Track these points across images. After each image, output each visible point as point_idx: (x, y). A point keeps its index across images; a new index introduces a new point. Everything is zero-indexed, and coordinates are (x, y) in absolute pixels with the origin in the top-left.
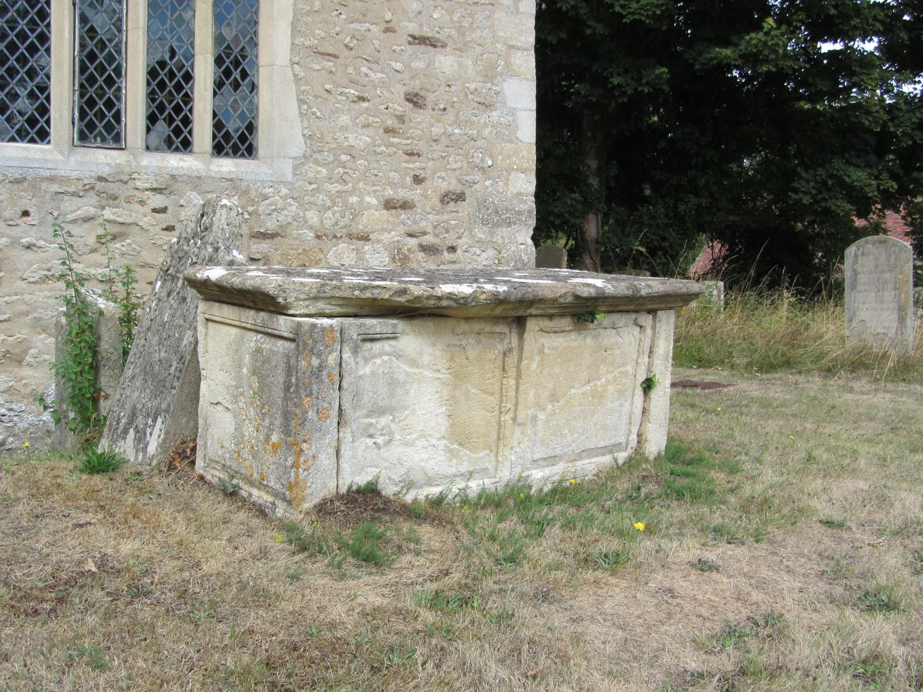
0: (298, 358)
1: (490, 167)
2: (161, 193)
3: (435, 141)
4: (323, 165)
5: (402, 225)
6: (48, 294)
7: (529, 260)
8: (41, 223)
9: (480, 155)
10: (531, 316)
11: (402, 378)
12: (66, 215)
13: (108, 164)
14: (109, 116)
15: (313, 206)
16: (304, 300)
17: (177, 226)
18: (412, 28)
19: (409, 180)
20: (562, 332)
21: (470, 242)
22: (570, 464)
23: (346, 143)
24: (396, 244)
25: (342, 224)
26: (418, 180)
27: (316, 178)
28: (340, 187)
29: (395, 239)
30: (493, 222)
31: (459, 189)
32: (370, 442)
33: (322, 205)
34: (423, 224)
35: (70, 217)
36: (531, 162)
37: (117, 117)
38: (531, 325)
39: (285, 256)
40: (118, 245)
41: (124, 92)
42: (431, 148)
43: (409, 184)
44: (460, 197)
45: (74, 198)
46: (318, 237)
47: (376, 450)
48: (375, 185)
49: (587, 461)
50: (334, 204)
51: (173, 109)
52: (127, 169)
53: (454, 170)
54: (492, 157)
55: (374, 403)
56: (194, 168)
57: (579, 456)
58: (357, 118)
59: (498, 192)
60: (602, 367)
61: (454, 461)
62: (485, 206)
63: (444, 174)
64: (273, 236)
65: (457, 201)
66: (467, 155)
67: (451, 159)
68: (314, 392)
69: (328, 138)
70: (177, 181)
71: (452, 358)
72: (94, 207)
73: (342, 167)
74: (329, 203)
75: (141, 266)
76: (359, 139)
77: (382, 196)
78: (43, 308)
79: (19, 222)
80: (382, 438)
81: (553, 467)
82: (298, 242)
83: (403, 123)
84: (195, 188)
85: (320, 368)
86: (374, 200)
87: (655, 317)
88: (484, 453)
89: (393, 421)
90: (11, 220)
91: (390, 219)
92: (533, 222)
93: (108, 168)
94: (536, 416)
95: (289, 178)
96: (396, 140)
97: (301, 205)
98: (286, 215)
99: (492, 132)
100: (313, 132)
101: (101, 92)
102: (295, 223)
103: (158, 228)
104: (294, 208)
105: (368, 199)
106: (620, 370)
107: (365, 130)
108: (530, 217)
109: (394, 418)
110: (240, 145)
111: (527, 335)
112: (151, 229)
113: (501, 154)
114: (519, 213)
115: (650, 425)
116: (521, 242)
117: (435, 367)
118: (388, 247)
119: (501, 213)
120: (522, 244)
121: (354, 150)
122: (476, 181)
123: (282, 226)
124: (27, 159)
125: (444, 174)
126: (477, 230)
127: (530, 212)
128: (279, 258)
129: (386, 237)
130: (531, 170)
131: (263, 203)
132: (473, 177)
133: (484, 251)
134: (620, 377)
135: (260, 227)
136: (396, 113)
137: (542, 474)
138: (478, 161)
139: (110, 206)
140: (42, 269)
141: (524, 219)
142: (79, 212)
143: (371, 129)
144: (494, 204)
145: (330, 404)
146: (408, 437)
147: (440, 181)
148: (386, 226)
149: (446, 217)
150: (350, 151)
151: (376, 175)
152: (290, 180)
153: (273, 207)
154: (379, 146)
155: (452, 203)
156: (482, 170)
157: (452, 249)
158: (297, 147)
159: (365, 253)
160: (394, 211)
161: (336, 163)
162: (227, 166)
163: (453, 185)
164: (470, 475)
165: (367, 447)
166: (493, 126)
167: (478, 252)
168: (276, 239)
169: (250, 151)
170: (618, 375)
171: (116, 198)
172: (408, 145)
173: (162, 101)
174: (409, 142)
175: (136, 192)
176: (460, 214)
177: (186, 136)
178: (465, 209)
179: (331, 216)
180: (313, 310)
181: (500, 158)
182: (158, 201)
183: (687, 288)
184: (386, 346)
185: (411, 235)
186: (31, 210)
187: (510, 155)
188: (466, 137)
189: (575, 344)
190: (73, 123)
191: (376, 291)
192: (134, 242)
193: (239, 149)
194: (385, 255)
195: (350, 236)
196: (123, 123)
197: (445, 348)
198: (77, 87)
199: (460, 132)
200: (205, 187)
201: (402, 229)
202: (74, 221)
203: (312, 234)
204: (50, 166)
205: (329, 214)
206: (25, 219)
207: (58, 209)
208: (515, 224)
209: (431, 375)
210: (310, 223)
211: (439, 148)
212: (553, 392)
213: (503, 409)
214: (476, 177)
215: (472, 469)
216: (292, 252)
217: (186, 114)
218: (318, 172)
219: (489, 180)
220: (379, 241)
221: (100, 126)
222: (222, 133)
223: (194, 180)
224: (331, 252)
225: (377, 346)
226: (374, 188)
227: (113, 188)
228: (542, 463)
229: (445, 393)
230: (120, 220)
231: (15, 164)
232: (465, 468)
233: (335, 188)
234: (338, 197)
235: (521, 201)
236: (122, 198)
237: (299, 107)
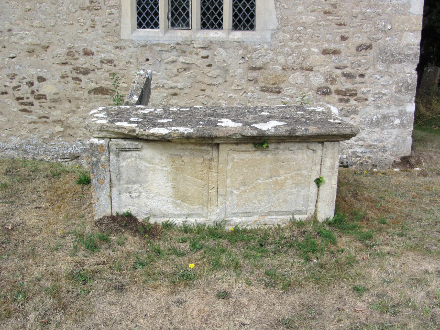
1: (389, 30)
2: (206, 49)
3: (355, 17)
4: (288, 33)
5: (333, 63)
6: (157, 94)
7: (413, 82)
8: (154, 64)
9: (383, 23)
10: (222, 143)
11: (143, 168)
12: (164, 60)
13: (182, 37)
14: (184, 14)
15: (282, 54)
16: (97, 131)
17: (213, 64)
19: (338, 38)
20: (249, 151)
21: (373, 72)
22: (260, 217)
23: (301, 21)
24: (328, 73)
25: (297, 62)
26: (343, 38)
27: (284, 40)
28: (297, 44)
29: (328, 70)
30: (389, 61)
31: (368, 43)
32: (128, 195)
33: (286, 53)
34: (345, 62)
35: (166, 61)
36: (418, 26)
37: (187, 15)
38: (221, 147)
39: (266, 78)
40: (187, 73)
41: (190, 3)
42: (353, 21)
43: (338, 41)
44: (369, 47)
45: (167, 53)
46: (284, 69)
47: (131, 199)
48: (318, 42)
49: (274, 217)
50: (293, 52)
51: (214, 9)
52: (190, 39)
53: (366, 32)
54: (391, 24)
55: (128, 179)
56: (221, 37)
57: (269, 214)
58: (308, 7)
59: (394, 44)
60: (281, 170)
61: (179, 208)
62: (385, 52)
63: (360, 35)
64: (259, 69)
65: (366, 49)
66: (375, 23)
67: (364, 26)
68: (95, 172)
69: (291, 18)
70: (213, 43)
71: (173, 161)
72: (176, 56)
73: (299, 33)
74: (290, 52)
75: (197, 82)
76: (310, 18)
77: (321, 48)
78: (155, 100)
79: (145, 63)
80: (135, 194)
81: (249, 218)
82: (273, 72)
83: (336, 8)
84: (221, 47)
85: (97, 162)
86: (317, 49)
87: (323, 145)
88: (198, 206)
89: (140, 187)
90: (142, 62)
91: (326, 59)
92: (417, 61)
93: (181, 39)
94: (232, 192)
95: (269, 40)
96: (331, 18)
97: (275, 53)
98: (267, 59)
99: (392, 10)
100: (282, 16)
101: (180, 4)
102: (271, 62)
103: (204, 65)
104: (271, 55)
105: (313, 49)
106: (296, 172)
107: (312, 13)
108: (415, 57)
109: (141, 186)
110: (246, 24)
111: (221, 152)
112: (201, 66)
113: (397, 22)
114: (407, 56)
115: (320, 203)
116: (407, 72)
117: (163, 165)
118: (324, 74)
119: (395, 55)
120: (409, 73)
121: (306, 24)
122: (380, 38)
123: (264, 64)
124: (147, 36)
125: (360, 35)
126: (378, 65)
127: (415, 55)
128: (262, 80)
129: (322, 69)
130: (418, 30)
131: (255, 53)
132: (377, 36)
133: (382, 77)
134: (296, 176)
135: (253, 64)
136: (331, 3)
137: (240, 220)
138: (381, 27)
139: (182, 56)
140: (155, 83)
141: (411, 59)
142: (169, 59)
143: (316, 13)
144: (391, 50)
145: (104, 177)
146: (150, 195)
147: (357, 38)
148: (323, 63)
149: (359, 58)
150: (303, 25)
151: (318, 37)
152: (269, 41)
153: (260, 55)
154: (320, 21)
155: (363, 51)
156: (384, 31)
157: (362, 76)
158: (274, 24)
159: (310, 77)
160: (328, 55)
161: (295, 31)
162: (238, 35)
163: (365, 41)
164: (189, 215)
165: (127, 197)
166: (393, 6)
167: (378, 77)
168: (261, 70)
169: (252, 27)
170: (294, 175)
171: (185, 52)
172: (338, 20)
173: (208, 6)
174: (339, 18)
175: (194, 49)
176: (368, 57)
177: (220, 22)
178: (371, 54)
179: (291, 58)
180: (101, 135)
181: (397, 24)
182: (204, 53)
183: (339, 131)
184: (134, 154)
185: (337, 68)
186: (149, 59)
187: (404, 23)
188: (375, 14)
189: (259, 158)
190: (168, 19)
191: (123, 130)
192: (194, 72)
193: (246, 26)
194: (322, 78)
195: (302, 69)
196: (190, 18)
197: (169, 156)
198: (170, 3)
199: (371, 11)
200: (226, 46)
201: (333, 65)
202: (167, 63)
203: (280, 68)
204: (157, 39)
205: (290, 57)
206: (147, 62)
207: (161, 57)
208: (404, 61)
209: (160, 168)
210: (279, 62)
211: (357, 20)
212: (243, 181)
213: (210, 187)
214: (380, 36)
215: (190, 213)
216: (269, 77)
217: (220, 11)
218: (285, 37)
219: (389, 37)
220: (318, 71)
221: (180, 19)
222: (237, 19)
223: (221, 43)
224: (291, 77)
225: (129, 154)
226: (317, 43)
227: (184, 48)
228: (241, 215)
229: (170, 177)
230: (187, 62)
231: (143, 39)
232: (185, 212)
233: (293, 44)
234: (296, 49)
235: (410, 49)
236: (188, 52)
237: (275, 4)
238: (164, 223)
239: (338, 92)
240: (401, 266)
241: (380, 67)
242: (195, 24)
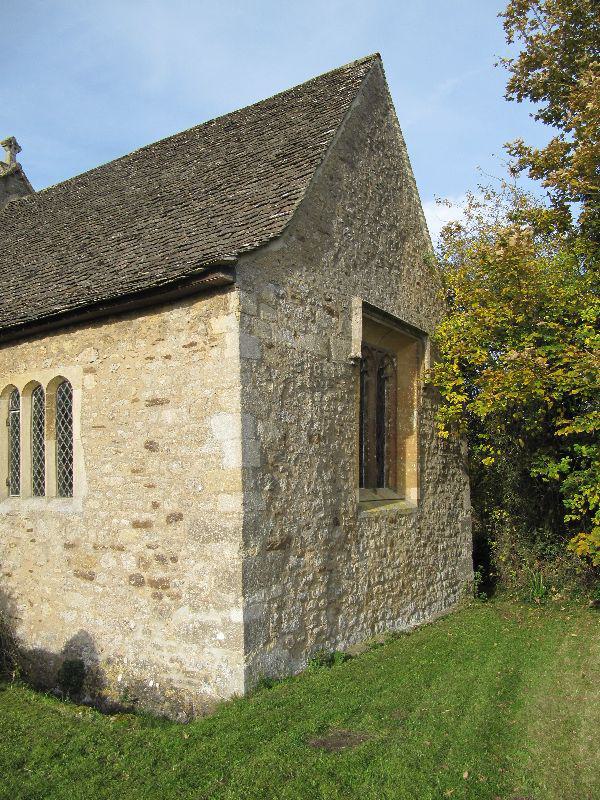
0: (255, 250)
18: (148, 395)
19: (150, 505)
76: (116, 481)
105: (123, 521)
178: (181, 528)
195: (112, 547)
239: (154, 584)
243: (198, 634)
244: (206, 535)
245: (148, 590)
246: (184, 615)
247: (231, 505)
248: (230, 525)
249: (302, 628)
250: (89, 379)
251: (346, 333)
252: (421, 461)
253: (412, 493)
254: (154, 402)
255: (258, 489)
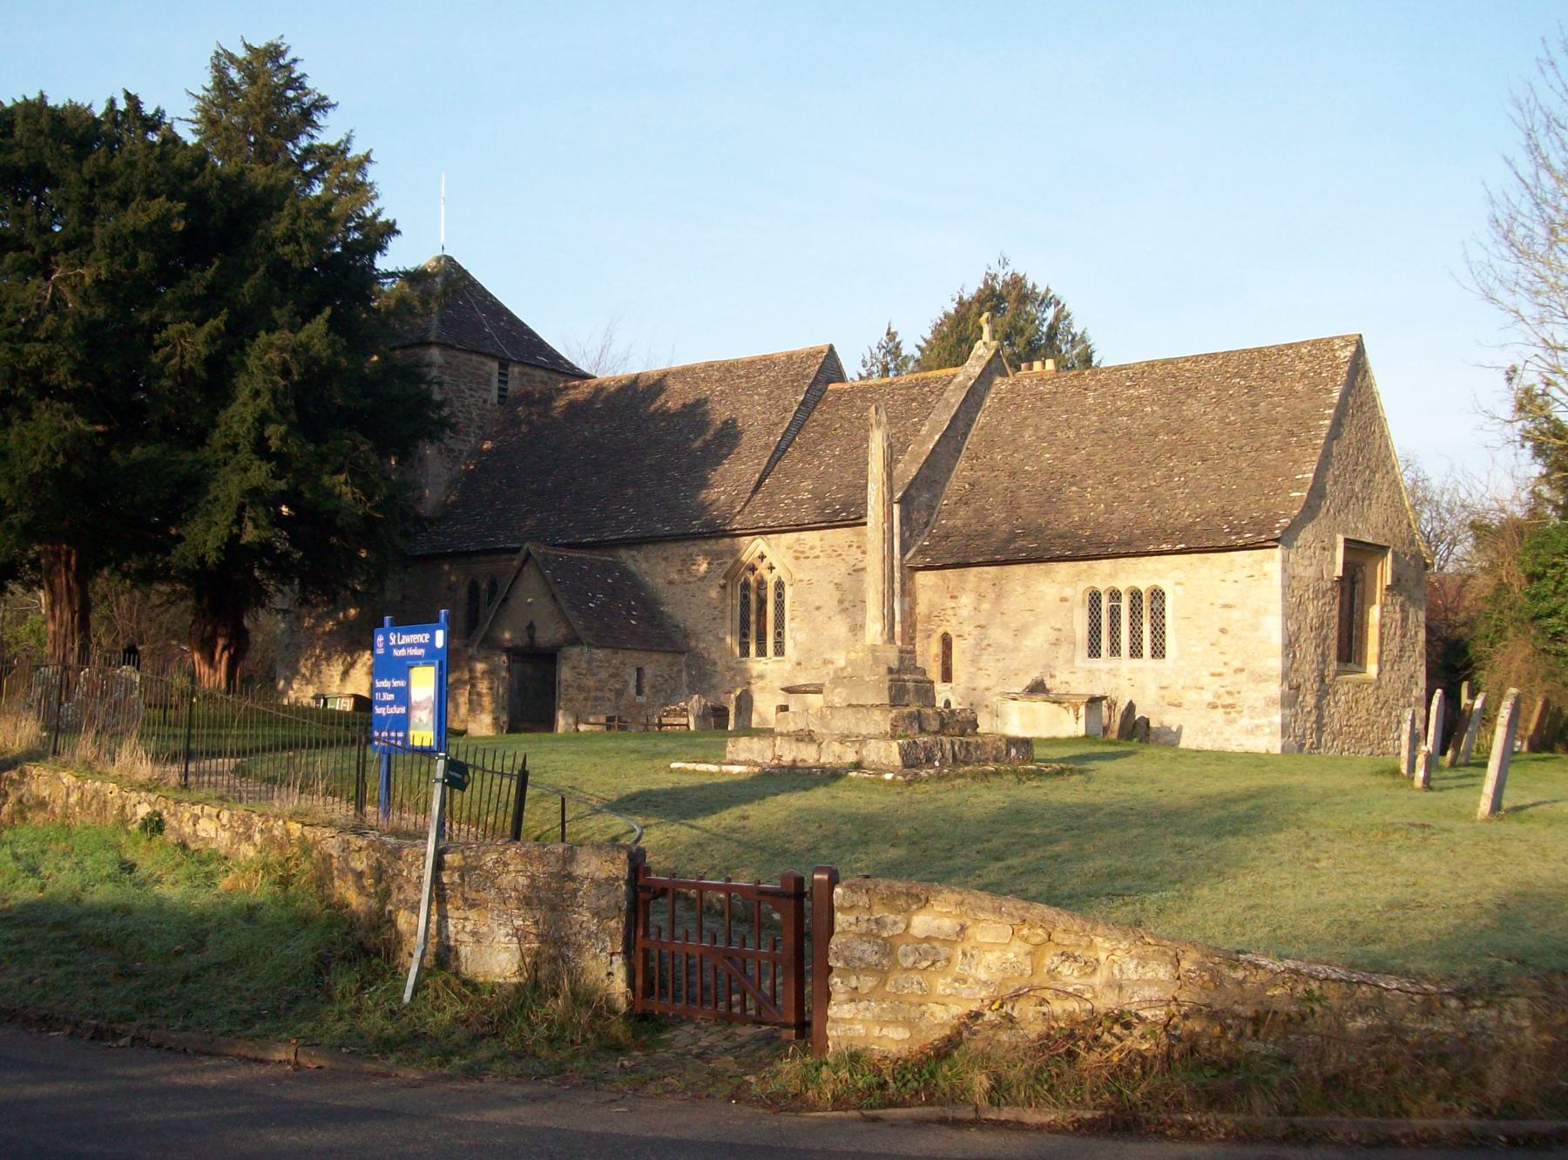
18: (1221, 602)
44: (1242, 670)
238: (166, 906)
239: (1225, 706)
240: (170, 1049)
241: (1252, 685)
242: (1122, 644)
243: (1253, 731)
244: (1259, 678)
245: (1221, 710)
246: (1245, 722)
247: (1275, 664)
248: (1274, 673)
249: (1304, 735)
250: (1178, 588)
251: (1333, 561)
252: (1381, 644)
253: (1372, 669)
254: (1226, 606)
255: (1288, 655)
